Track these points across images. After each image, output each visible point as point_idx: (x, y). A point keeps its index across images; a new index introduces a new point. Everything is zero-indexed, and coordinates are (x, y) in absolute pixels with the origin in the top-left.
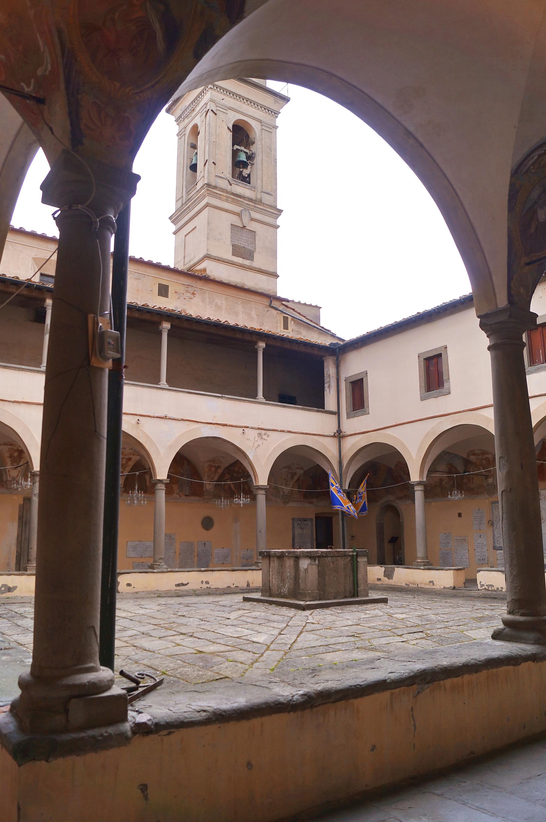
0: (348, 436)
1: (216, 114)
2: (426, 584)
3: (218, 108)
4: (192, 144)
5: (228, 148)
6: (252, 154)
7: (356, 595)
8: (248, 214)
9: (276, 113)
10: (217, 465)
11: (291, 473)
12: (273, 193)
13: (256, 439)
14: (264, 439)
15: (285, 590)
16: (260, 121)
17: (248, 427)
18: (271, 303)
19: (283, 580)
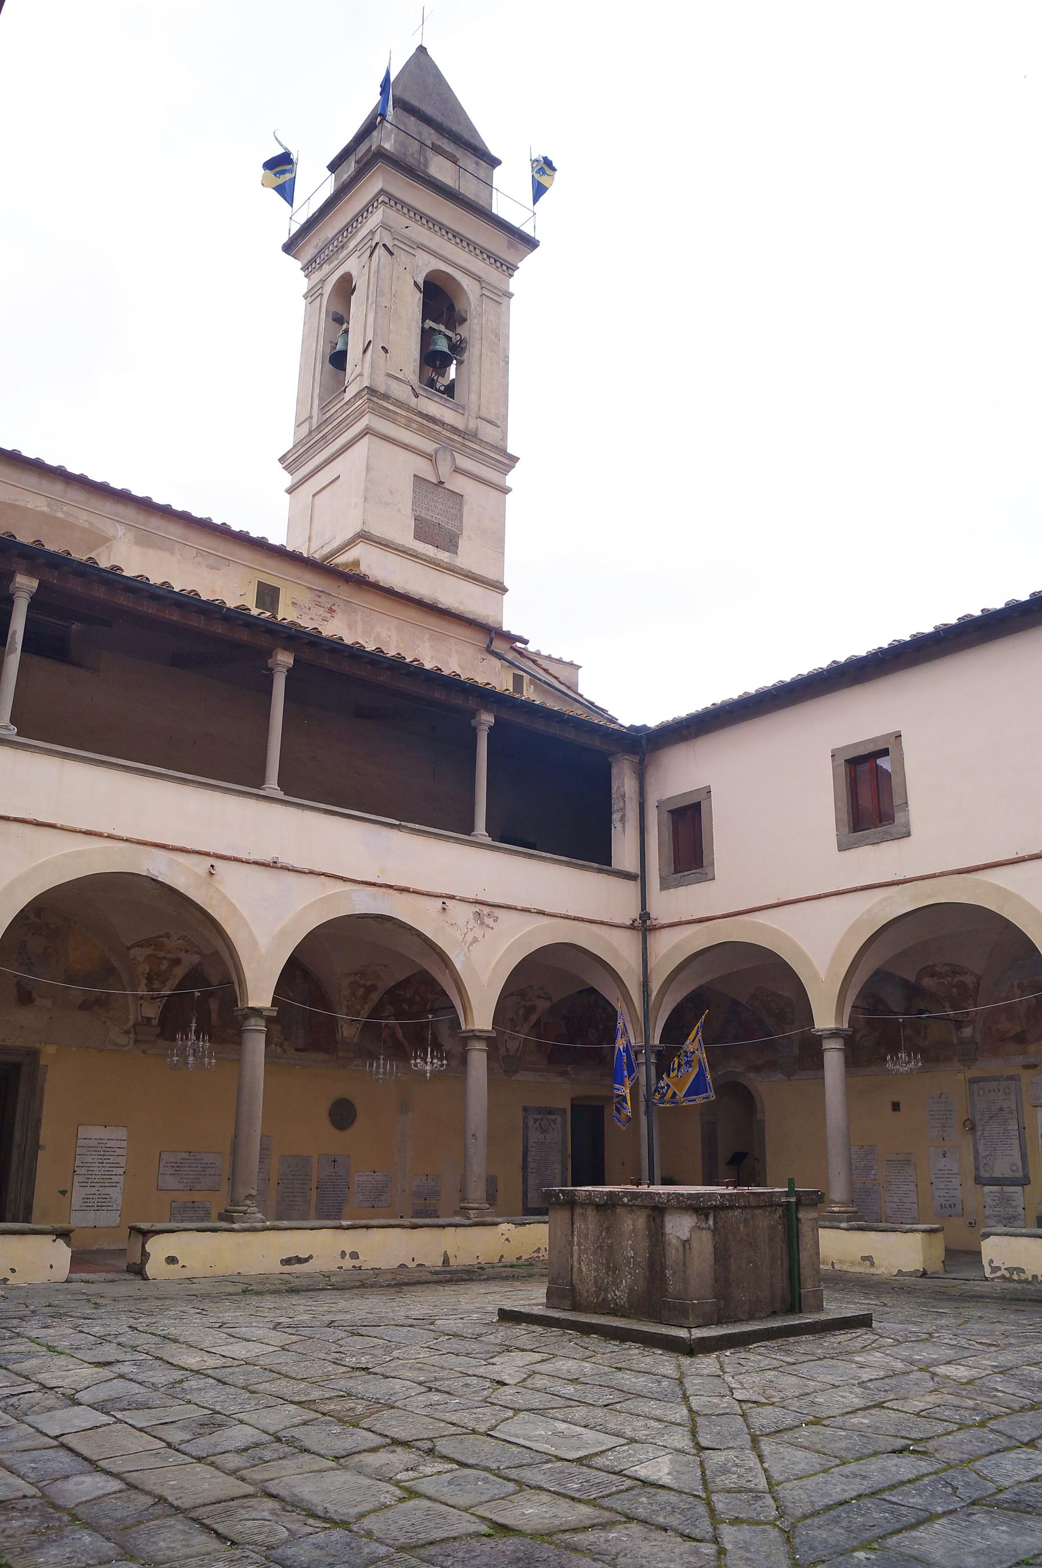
0: (663, 927)
1: (391, 254)
2: (853, 1263)
3: (396, 242)
4: (335, 313)
5: (414, 323)
6: (461, 341)
7: (797, 1310)
8: (449, 457)
9: (510, 269)
10: (369, 983)
11: (525, 1006)
12: (500, 423)
13: (470, 926)
14: (488, 926)
15: (620, 1294)
16: (478, 279)
17: (453, 897)
18: (491, 642)
19: (613, 1269)
